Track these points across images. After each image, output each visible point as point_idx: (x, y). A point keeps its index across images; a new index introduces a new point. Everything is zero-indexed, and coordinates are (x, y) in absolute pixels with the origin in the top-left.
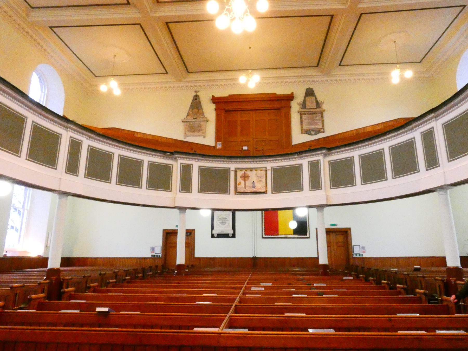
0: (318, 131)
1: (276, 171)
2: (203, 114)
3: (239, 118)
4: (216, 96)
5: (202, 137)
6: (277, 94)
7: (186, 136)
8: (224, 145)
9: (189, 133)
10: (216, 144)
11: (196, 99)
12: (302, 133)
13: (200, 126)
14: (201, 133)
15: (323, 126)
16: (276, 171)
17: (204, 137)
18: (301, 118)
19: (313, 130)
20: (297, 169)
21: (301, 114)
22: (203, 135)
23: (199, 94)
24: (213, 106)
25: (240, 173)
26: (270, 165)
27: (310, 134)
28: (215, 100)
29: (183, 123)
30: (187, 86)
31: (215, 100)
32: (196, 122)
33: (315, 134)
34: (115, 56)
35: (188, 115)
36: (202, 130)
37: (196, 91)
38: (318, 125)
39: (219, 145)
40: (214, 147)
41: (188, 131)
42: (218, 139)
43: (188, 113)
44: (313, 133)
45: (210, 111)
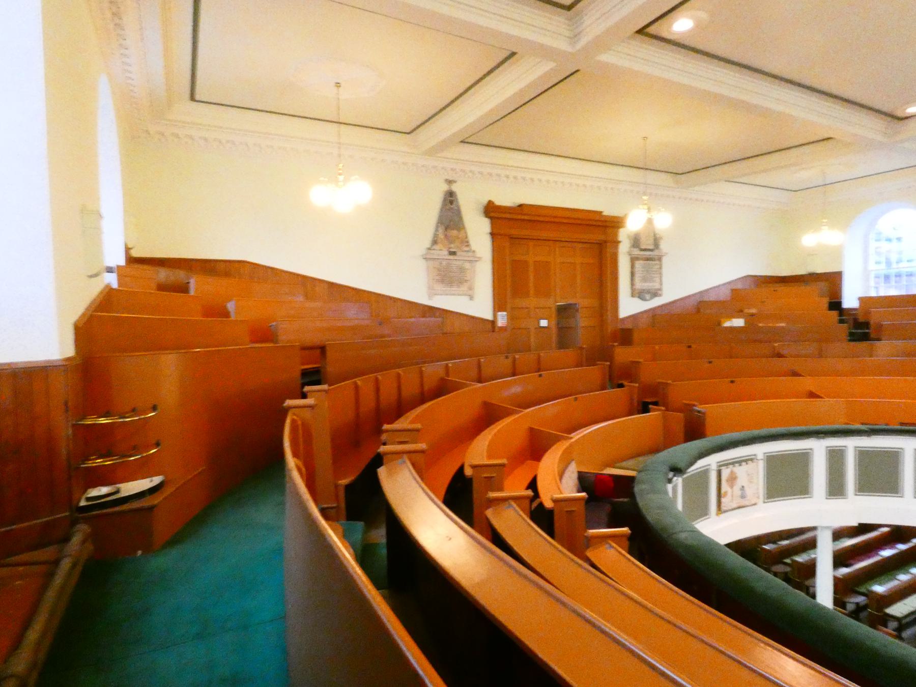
0: (655, 294)
1: (772, 461)
2: (467, 242)
3: (533, 255)
4: (499, 202)
5: (466, 298)
6: (604, 214)
7: (432, 293)
8: (511, 318)
9: (439, 287)
10: (495, 316)
11: (451, 202)
12: (633, 296)
13: (462, 270)
14: (464, 288)
15: (661, 284)
16: (772, 461)
17: (471, 298)
18: (633, 266)
19: (648, 292)
20: (804, 458)
21: (633, 260)
22: (470, 292)
23: (454, 188)
24: (485, 225)
25: (726, 473)
26: (760, 450)
27: (644, 299)
28: (491, 211)
29: (424, 261)
30: (435, 167)
31: (491, 211)
32: (455, 262)
33: (651, 298)
34: (338, 85)
35: (435, 242)
36: (466, 281)
37: (450, 182)
38: (654, 281)
39: (502, 319)
40: (493, 323)
41: (438, 281)
42: (499, 304)
43: (436, 236)
44: (648, 296)
45: (479, 232)
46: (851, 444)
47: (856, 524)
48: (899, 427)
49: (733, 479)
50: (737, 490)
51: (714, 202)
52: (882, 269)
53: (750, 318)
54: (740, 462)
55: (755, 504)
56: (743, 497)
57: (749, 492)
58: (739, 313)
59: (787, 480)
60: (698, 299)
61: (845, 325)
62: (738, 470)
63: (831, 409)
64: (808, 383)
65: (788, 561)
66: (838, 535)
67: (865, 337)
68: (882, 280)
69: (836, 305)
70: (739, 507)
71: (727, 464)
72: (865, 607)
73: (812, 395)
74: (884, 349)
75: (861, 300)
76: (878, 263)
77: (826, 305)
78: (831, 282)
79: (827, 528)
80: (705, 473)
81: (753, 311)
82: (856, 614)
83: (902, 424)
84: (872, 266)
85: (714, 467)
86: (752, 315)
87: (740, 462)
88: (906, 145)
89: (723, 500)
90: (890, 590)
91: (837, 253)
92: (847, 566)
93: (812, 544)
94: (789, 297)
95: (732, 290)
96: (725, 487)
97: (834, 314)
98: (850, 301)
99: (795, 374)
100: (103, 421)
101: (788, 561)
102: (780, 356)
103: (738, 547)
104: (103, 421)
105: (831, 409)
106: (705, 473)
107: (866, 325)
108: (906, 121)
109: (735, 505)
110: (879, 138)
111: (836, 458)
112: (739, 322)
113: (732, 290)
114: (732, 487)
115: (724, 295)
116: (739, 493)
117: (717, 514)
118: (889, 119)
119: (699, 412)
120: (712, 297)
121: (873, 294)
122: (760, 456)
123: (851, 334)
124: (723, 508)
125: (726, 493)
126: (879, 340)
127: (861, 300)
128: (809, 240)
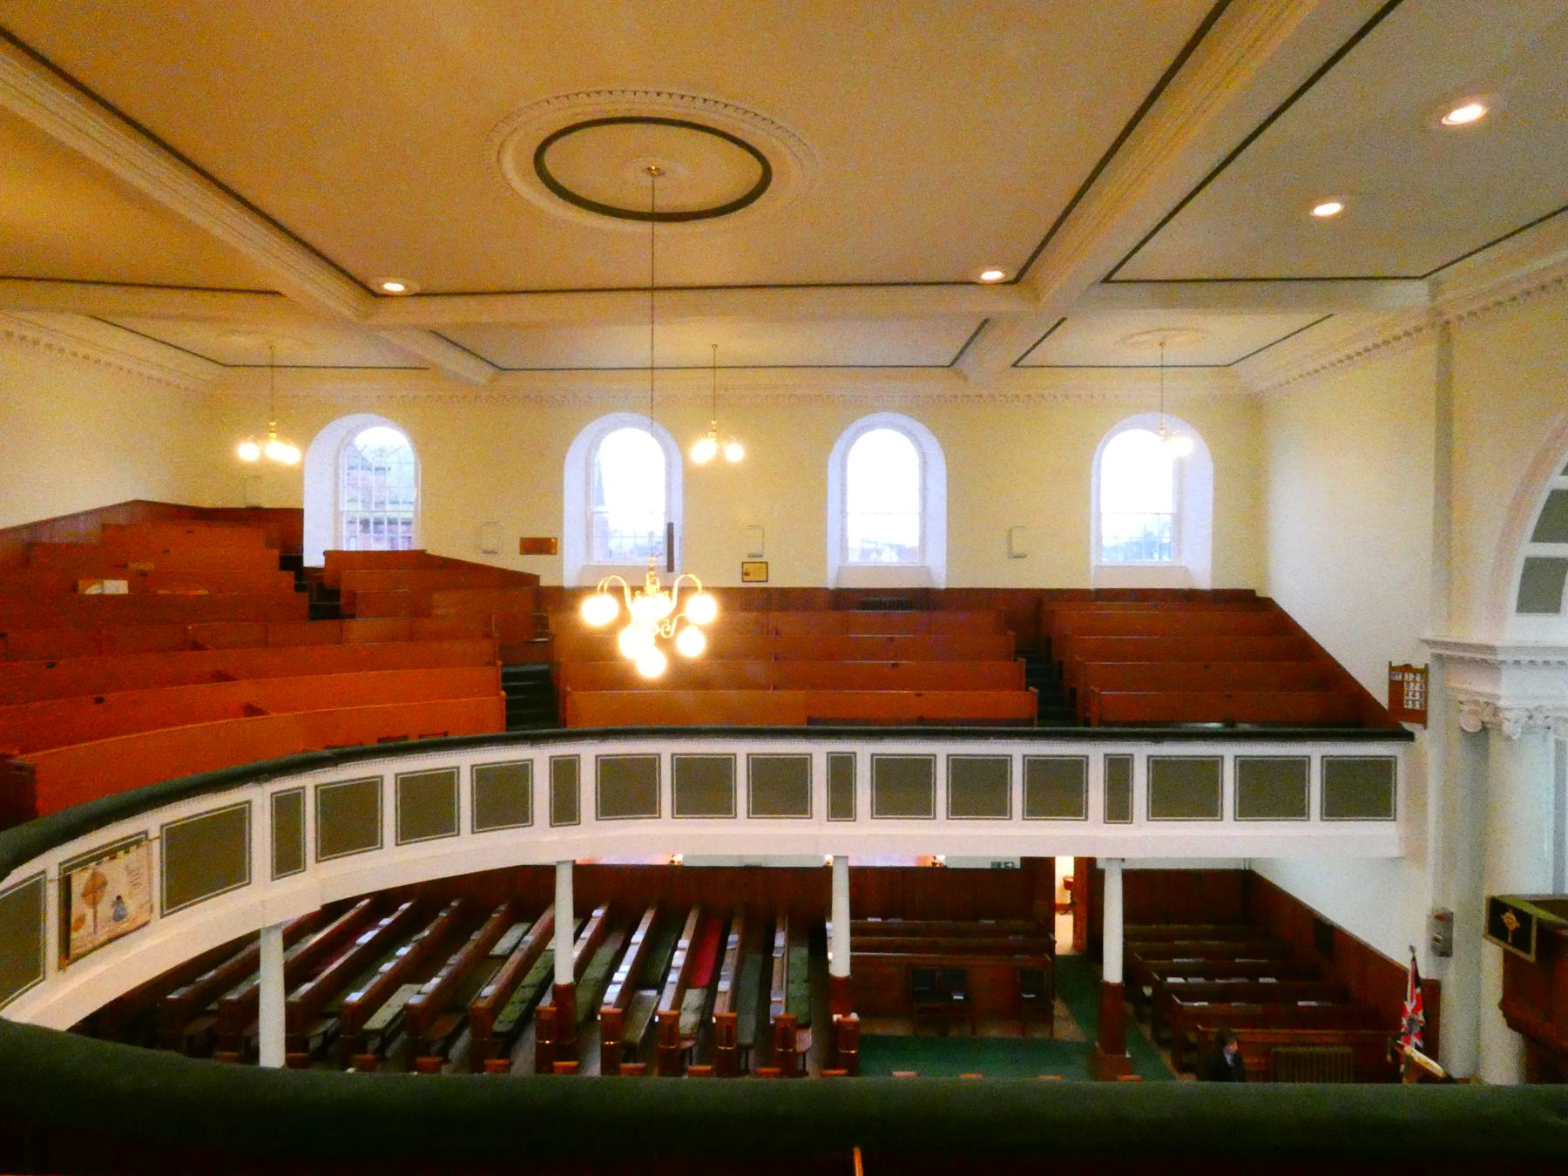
12: (1392, 669)
25: (80, 881)
26: (153, 822)
46: (308, 783)
47: (317, 908)
48: (376, 745)
49: (95, 890)
50: (105, 908)
51: (49, 346)
52: (359, 510)
53: (140, 582)
54: (110, 852)
55: (145, 924)
56: (119, 917)
57: (131, 905)
58: (116, 571)
59: (203, 864)
60: (25, 535)
61: (306, 594)
62: (107, 868)
63: (281, 730)
64: (245, 691)
65: (214, 1006)
66: (293, 935)
67: (335, 613)
68: (358, 527)
69: (291, 558)
70: (110, 941)
71: (82, 862)
72: (337, 1033)
73: (251, 710)
74: (359, 628)
75: (328, 554)
76: (353, 500)
77: (276, 563)
78: (285, 525)
79: (276, 927)
80: (32, 893)
81: (148, 566)
82: (321, 1056)
83: (380, 740)
84: (345, 506)
85: (54, 874)
86: (144, 574)
87: (110, 852)
88: (383, 334)
89: (74, 935)
90: (368, 993)
91: (295, 477)
92: (310, 980)
93: (252, 965)
94: (225, 546)
95: (104, 527)
96: (79, 907)
97: (288, 577)
98: (313, 557)
99: (222, 677)
100: (679, 959)
101: (214, 1006)
102: (197, 646)
103: (93, 1025)
104: (679, 959)
105: (281, 730)
106: (32, 893)
107: (336, 594)
108: (383, 301)
109: (104, 938)
110: (347, 312)
111: (287, 808)
112: (117, 587)
113: (104, 527)
114: (94, 904)
115: (88, 532)
116: (110, 912)
117: (61, 967)
118: (360, 291)
119: (19, 768)
120: (61, 537)
121: (353, 545)
122: (154, 833)
123: (312, 608)
124: (74, 952)
125: (82, 920)
126: (352, 616)
127: (328, 554)
128: (247, 452)
